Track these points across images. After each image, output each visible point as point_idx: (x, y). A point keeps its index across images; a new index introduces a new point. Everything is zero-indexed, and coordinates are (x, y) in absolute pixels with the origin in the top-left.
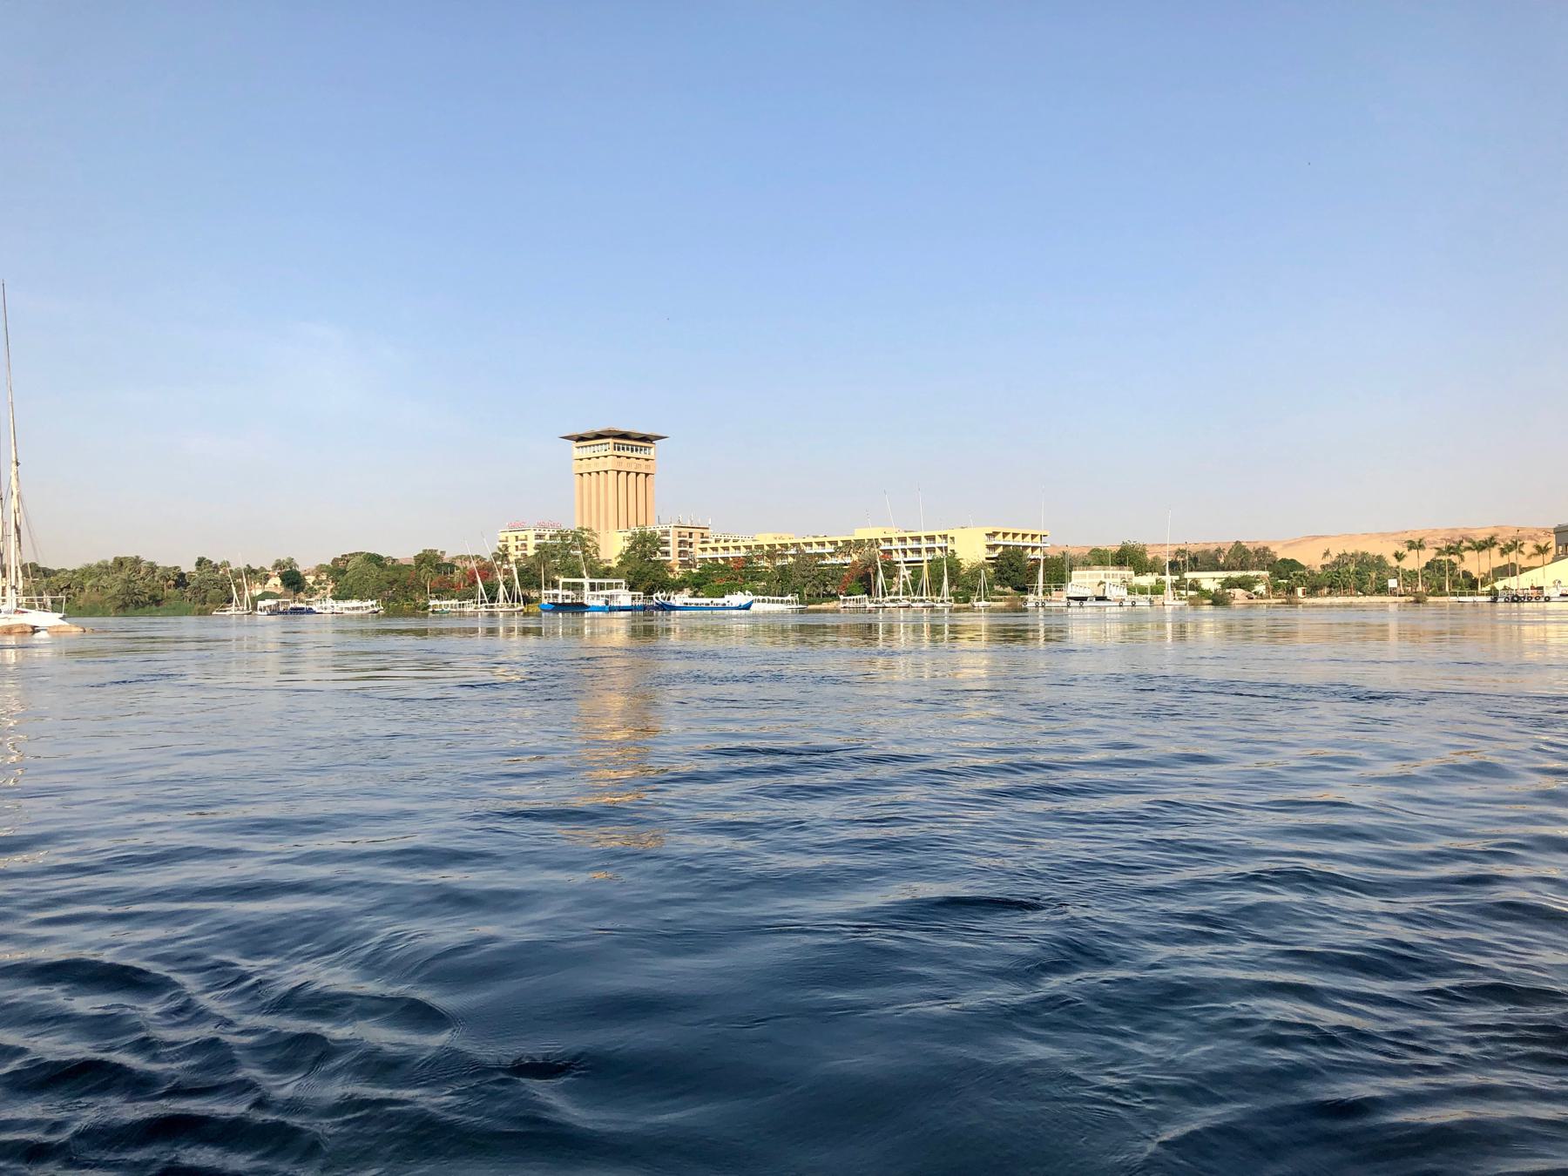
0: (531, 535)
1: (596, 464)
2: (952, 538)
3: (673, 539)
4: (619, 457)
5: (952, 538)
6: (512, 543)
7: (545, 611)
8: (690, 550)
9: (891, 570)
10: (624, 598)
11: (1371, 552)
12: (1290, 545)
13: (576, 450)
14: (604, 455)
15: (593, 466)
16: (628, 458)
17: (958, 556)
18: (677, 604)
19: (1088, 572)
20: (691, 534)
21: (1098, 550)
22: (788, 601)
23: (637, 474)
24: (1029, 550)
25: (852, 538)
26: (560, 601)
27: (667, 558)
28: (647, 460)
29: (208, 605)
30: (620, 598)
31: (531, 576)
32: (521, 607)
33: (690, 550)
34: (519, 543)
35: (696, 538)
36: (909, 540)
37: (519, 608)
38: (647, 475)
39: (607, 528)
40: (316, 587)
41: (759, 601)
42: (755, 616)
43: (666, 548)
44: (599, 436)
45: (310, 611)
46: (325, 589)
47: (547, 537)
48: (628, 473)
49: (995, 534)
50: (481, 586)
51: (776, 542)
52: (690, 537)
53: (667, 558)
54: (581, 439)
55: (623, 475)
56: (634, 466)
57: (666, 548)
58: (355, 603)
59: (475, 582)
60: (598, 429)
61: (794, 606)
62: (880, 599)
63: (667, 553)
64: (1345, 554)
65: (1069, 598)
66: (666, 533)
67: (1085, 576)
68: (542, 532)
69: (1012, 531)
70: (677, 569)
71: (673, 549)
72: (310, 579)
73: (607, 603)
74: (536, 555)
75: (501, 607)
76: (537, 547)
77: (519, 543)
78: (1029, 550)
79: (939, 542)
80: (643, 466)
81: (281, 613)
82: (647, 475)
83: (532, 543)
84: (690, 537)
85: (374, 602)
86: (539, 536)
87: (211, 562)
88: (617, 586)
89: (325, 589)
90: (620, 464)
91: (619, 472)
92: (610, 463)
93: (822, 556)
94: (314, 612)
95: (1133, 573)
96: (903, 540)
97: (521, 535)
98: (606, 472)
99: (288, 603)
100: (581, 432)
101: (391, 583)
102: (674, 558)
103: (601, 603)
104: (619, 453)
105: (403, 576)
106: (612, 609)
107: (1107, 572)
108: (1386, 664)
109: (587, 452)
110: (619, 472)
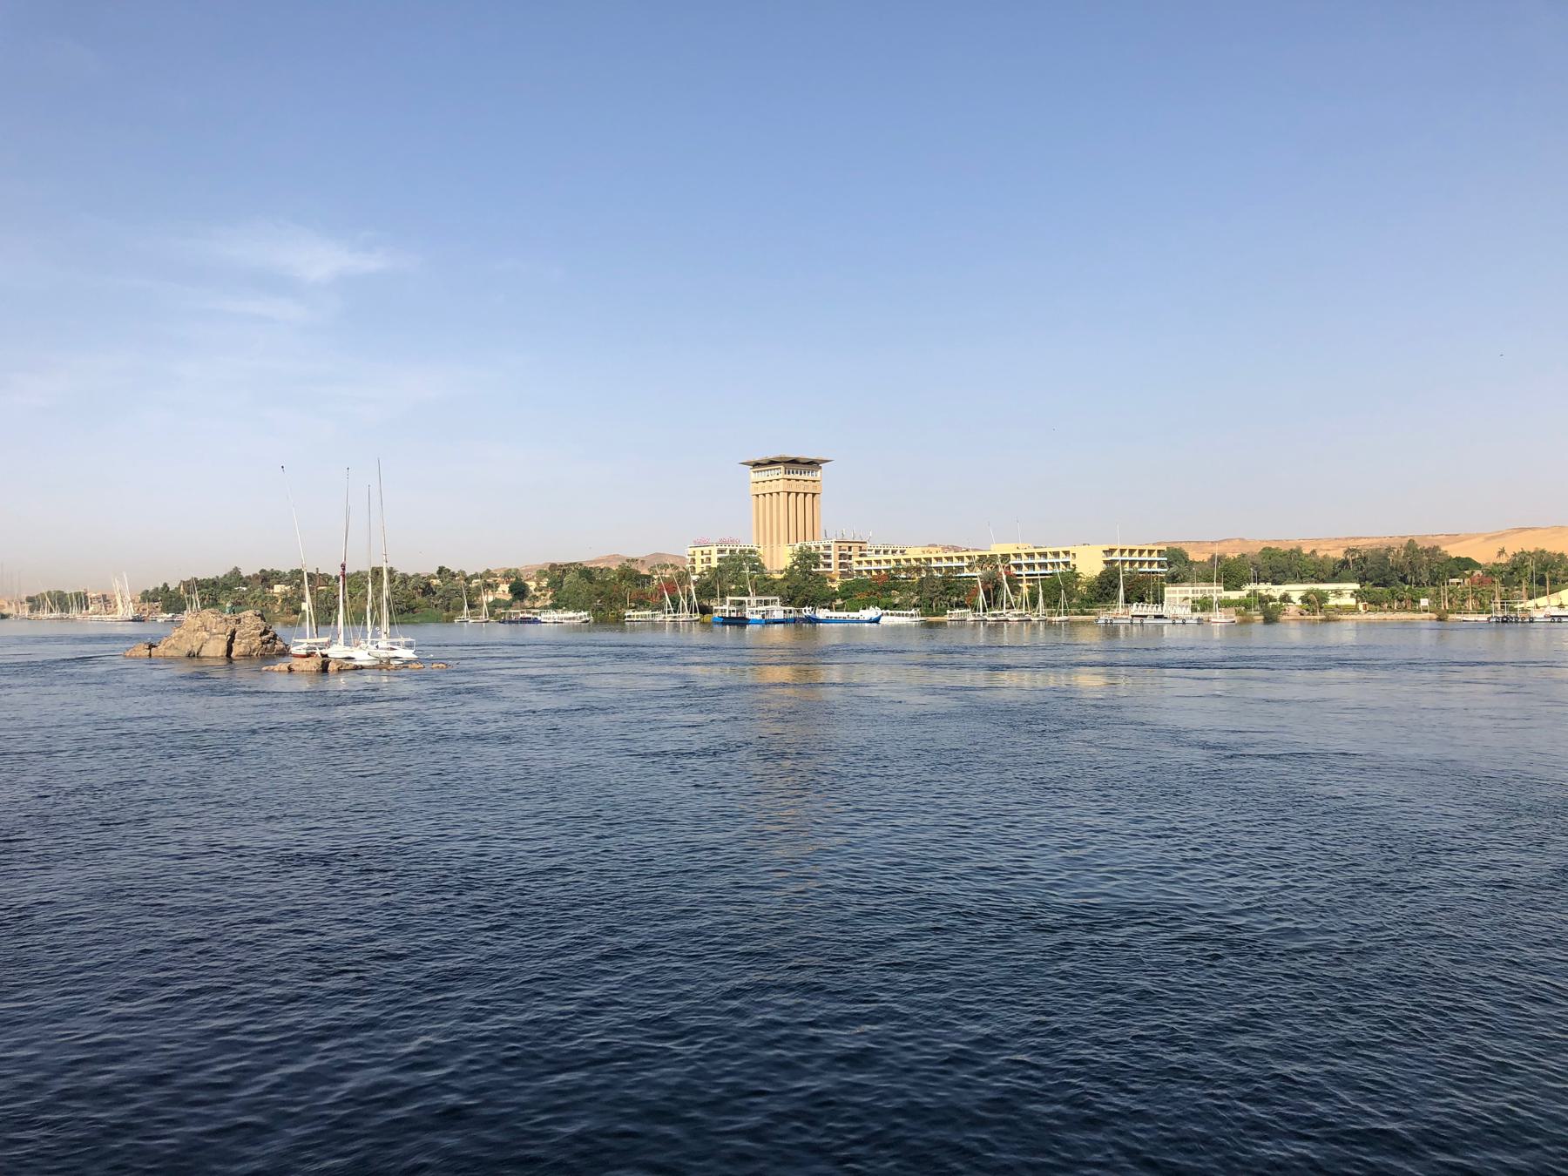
0: (714, 550)
1: (770, 487)
2: (1074, 554)
5: (1074, 554)
6: (698, 557)
9: (1014, 583)
10: (778, 612)
11: (1548, 550)
12: (1493, 538)
13: (754, 476)
15: (767, 488)
16: (798, 480)
17: (1078, 571)
18: (821, 618)
19: (1178, 589)
20: (850, 548)
21: (1270, 549)
22: (912, 615)
23: (805, 494)
24: (1127, 565)
25: (987, 553)
27: (829, 570)
28: (814, 481)
29: (451, 613)
30: (775, 613)
31: (708, 589)
32: (698, 616)
34: (704, 557)
35: (855, 551)
36: (1037, 556)
37: (697, 618)
38: (814, 495)
39: (779, 542)
40: (538, 594)
41: (887, 614)
42: (885, 628)
43: (828, 561)
44: (772, 462)
45: (536, 621)
46: (545, 595)
47: (728, 551)
48: (797, 494)
49: (1111, 551)
50: (668, 599)
51: (922, 556)
53: (829, 570)
54: (757, 464)
55: (793, 496)
56: (802, 487)
57: (828, 561)
58: (571, 614)
59: (663, 596)
60: (771, 457)
61: (918, 619)
62: (1004, 611)
63: (829, 565)
64: (1523, 552)
65: (1133, 616)
66: (828, 547)
67: (1174, 592)
69: (1120, 547)
70: (838, 579)
72: (532, 585)
73: (763, 616)
74: (719, 567)
75: (684, 616)
76: (720, 559)
77: (704, 557)
78: (1127, 565)
79: (1062, 558)
80: (811, 487)
81: (513, 622)
82: (814, 495)
83: (715, 556)
85: (586, 613)
86: (721, 551)
89: (545, 595)
90: (791, 485)
91: (789, 493)
92: (781, 486)
93: (961, 569)
94: (540, 622)
95: (1222, 588)
96: (1031, 555)
97: (706, 550)
98: (778, 493)
99: (517, 613)
100: (757, 459)
102: (835, 569)
103: (758, 617)
104: (787, 476)
105: (608, 589)
106: (768, 622)
107: (1195, 588)
108: (596, 676)
109: (762, 476)
110: (789, 493)
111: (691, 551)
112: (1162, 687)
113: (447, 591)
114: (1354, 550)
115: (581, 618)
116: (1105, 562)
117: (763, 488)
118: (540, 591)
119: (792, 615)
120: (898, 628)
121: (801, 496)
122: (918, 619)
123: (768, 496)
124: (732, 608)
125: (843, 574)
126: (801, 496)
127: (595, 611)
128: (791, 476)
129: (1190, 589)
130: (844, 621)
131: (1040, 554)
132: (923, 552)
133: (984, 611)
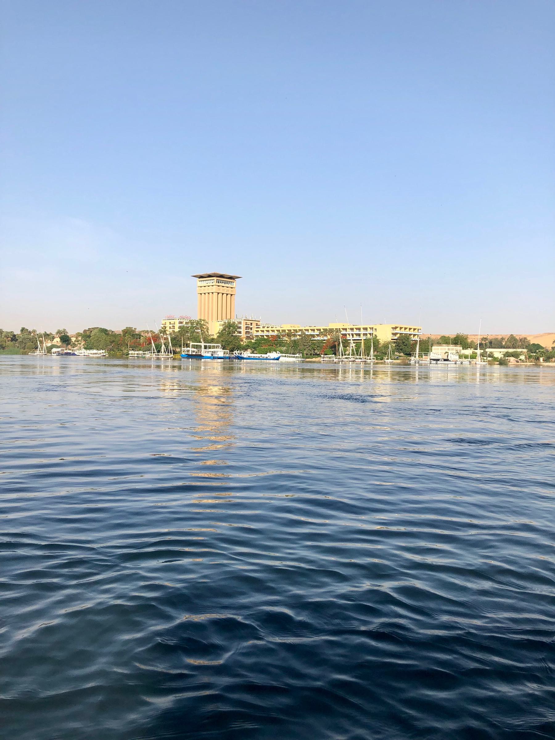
0: (177, 322)
2: (376, 329)
3: (243, 326)
4: (219, 286)
5: (376, 329)
6: (168, 325)
7: (184, 358)
8: (251, 331)
9: (346, 344)
12: (537, 337)
14: (212, 285)
15: (207, 290)
17: (378, 338)
18: (245, 357)
21: (444, 337)
22: (297, 357)
23: (227, 294)
25: (328, 328)
26: (190, 353)
27: (240, 335)
28: (232, 288)
33: (251, 331)
34: (171, 326)
35: (254, 326)
37: (171, 356)
38: (231, 295)
39: (212, 320)
40: (76, 343)
42: (282, 364)
43: (240, 330)
44: (210, 276)
45: (74, 354)
46: (80, 344)
47: (184, 323)
48: (223, 294)
49: (396, 328)
50: (153, 345)
51: (292, 329)
52: (251, 325)
53: (240, 335)
54: (201, 277)
55: (220, 295)
56: (226, 290)
57: (240, 330)
60: (209, 273)
63: (240, 332)
65: (431, 359)
68: (182, 321)
70: (244, 340)
71: (243, 330)
72: (73, 339)
73: (212, 355)
75: (162, 355)
76: (180, 327)
77: (171, 326)
79: (369, 331)
83: (177, 326)
84: (251, 325)
85: (104, 351)
86: (181, 323)
87: (27, 330)
88: (217, 347)
89: (80, 344)
91: (218, 293)
92: (215, 289)
93: (313, 336)
94: (76, 355)
96: (352, 329)
97: (172, 322)
98: (213, 293)
101: (112, 342)
102: (243, 335)
103: (209, 355)
104: (219, 284)
106: (214, 358)
107: (449, 347)
110: (218, 293)
111: (163, 322)
112: (312, 400)
113: (24, 339)
114: (485, 338)
115: (100, 353)
116: (393, 334)
117: (204, 290)
118: (78, 342)
119: (228, 355)
120: (288, 363)
121: (225, 295)
122: (300, 359)
123: (207, 294)
124: (193, 349)
125: (248, 338)
126: (225, 295)
127: (110, 351)
128: (220, 284)
129: (447, 348)
130: (259, 359)
131: (357, 329)
132: (291, 327)
133: (342, 355)
